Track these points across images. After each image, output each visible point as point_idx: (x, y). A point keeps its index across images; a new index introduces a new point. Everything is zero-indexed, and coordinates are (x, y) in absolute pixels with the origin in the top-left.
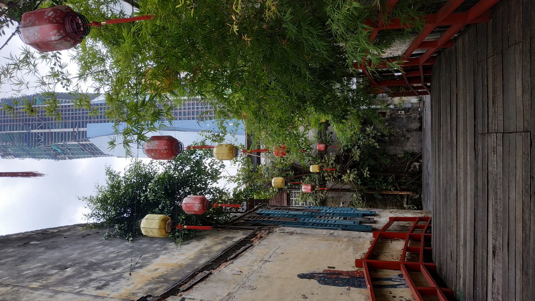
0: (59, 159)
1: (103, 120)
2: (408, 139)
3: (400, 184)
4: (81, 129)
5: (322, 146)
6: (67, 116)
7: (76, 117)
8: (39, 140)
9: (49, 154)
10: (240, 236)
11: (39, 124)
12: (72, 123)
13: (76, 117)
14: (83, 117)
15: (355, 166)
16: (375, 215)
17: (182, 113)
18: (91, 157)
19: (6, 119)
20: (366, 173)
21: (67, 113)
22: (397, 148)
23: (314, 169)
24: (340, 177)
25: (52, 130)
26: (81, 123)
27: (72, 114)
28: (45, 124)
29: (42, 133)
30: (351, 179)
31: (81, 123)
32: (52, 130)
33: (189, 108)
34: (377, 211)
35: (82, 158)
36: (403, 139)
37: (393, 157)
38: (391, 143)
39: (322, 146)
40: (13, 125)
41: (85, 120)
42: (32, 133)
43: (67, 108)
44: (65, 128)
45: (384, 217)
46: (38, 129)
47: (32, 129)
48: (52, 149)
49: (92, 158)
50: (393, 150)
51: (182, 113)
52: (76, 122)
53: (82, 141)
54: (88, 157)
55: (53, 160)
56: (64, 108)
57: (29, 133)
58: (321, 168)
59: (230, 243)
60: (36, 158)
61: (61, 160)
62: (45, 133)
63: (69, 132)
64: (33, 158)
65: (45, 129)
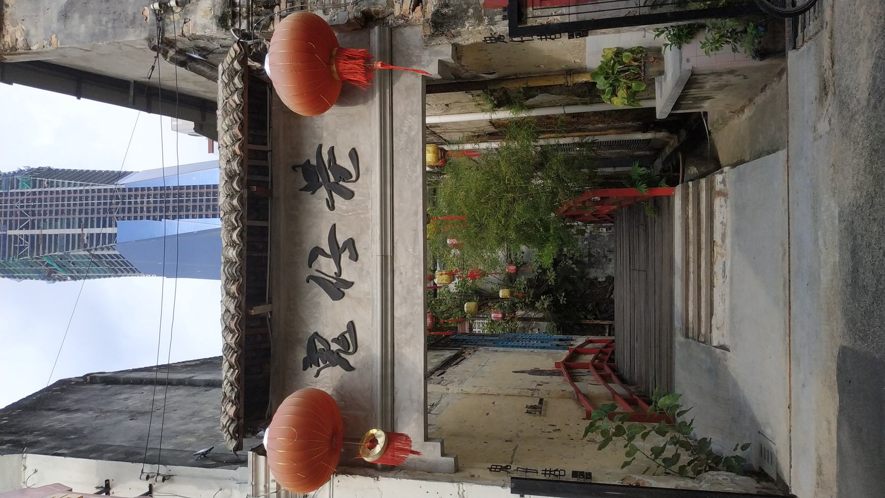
0: (55, 280)
1: (133, 214)
2: (610, 260)
3: (601, 312)
4: (108, 230)
5: (513, 268)
6: (72, 208)
7: (86, 210)
8: (21, 248)
9: (39, 272)
10: (448, 354)
11: (22, 222)
12: (80, 219)
13: (86, 210)
14: (135, 208)
15: (549, 291)
16: (572, 340)
17: (145, 209)
18: (110, 276)
19: (14, 209)
20: (562, 300)
21: (72, 202)
22: (598, 270)
23: (502, 293)
24: (533, 303)
25: (45, 232)
26: (95, 220)
27: (81, 205)
28: (33, 221)
29: (27, 236)
30: (546, 306)
31: (95, 220)
32: (45, 232)
33: (195, 201)
34: (574, 337)
35: (94, 277)
36: (604, 260)
37: (593, 282)
38: (591, 265)
39: (513, 268)
40: (10, 221)
41: (54, 216)
42: (10, 236)
43: (72, 195)
44: (68, 227)
45: (579, 341)
46: (21, 229)
47: (11, 229)
48: (43, 262)
49: (112, 279)
50: (593, 273)
51: (145, 209)
52: (87, 219)
53: (102, 249)
54: (105, 277)
55: (45, 282)
56: (72, 195)
57: (5, 235)
58: (512, 293)
59: (443, 358)
60: (14, 277)
61: (57, 282)
62: (32, 236)
63: (74, 235)
64: (9, 277)
65: (33, 228)
